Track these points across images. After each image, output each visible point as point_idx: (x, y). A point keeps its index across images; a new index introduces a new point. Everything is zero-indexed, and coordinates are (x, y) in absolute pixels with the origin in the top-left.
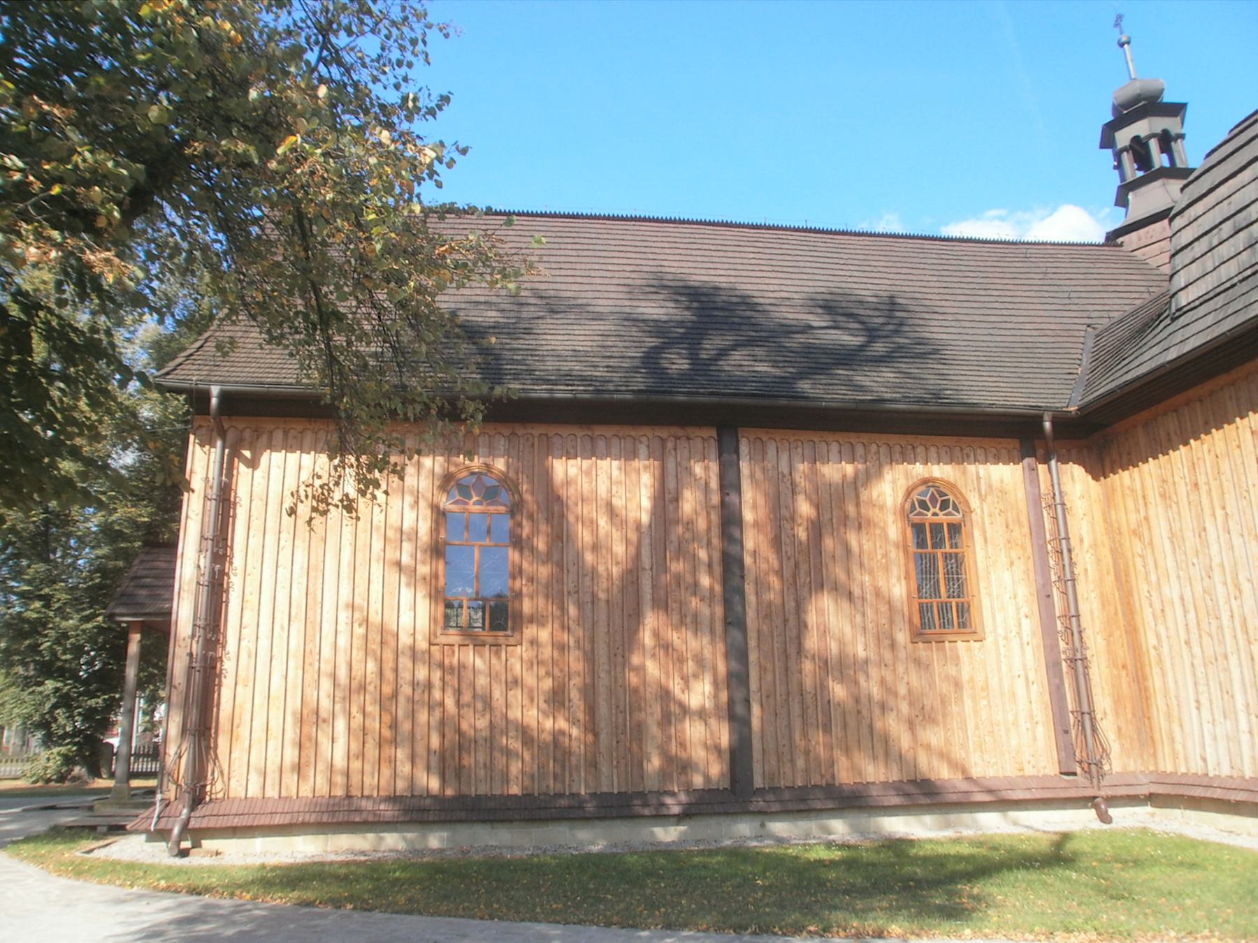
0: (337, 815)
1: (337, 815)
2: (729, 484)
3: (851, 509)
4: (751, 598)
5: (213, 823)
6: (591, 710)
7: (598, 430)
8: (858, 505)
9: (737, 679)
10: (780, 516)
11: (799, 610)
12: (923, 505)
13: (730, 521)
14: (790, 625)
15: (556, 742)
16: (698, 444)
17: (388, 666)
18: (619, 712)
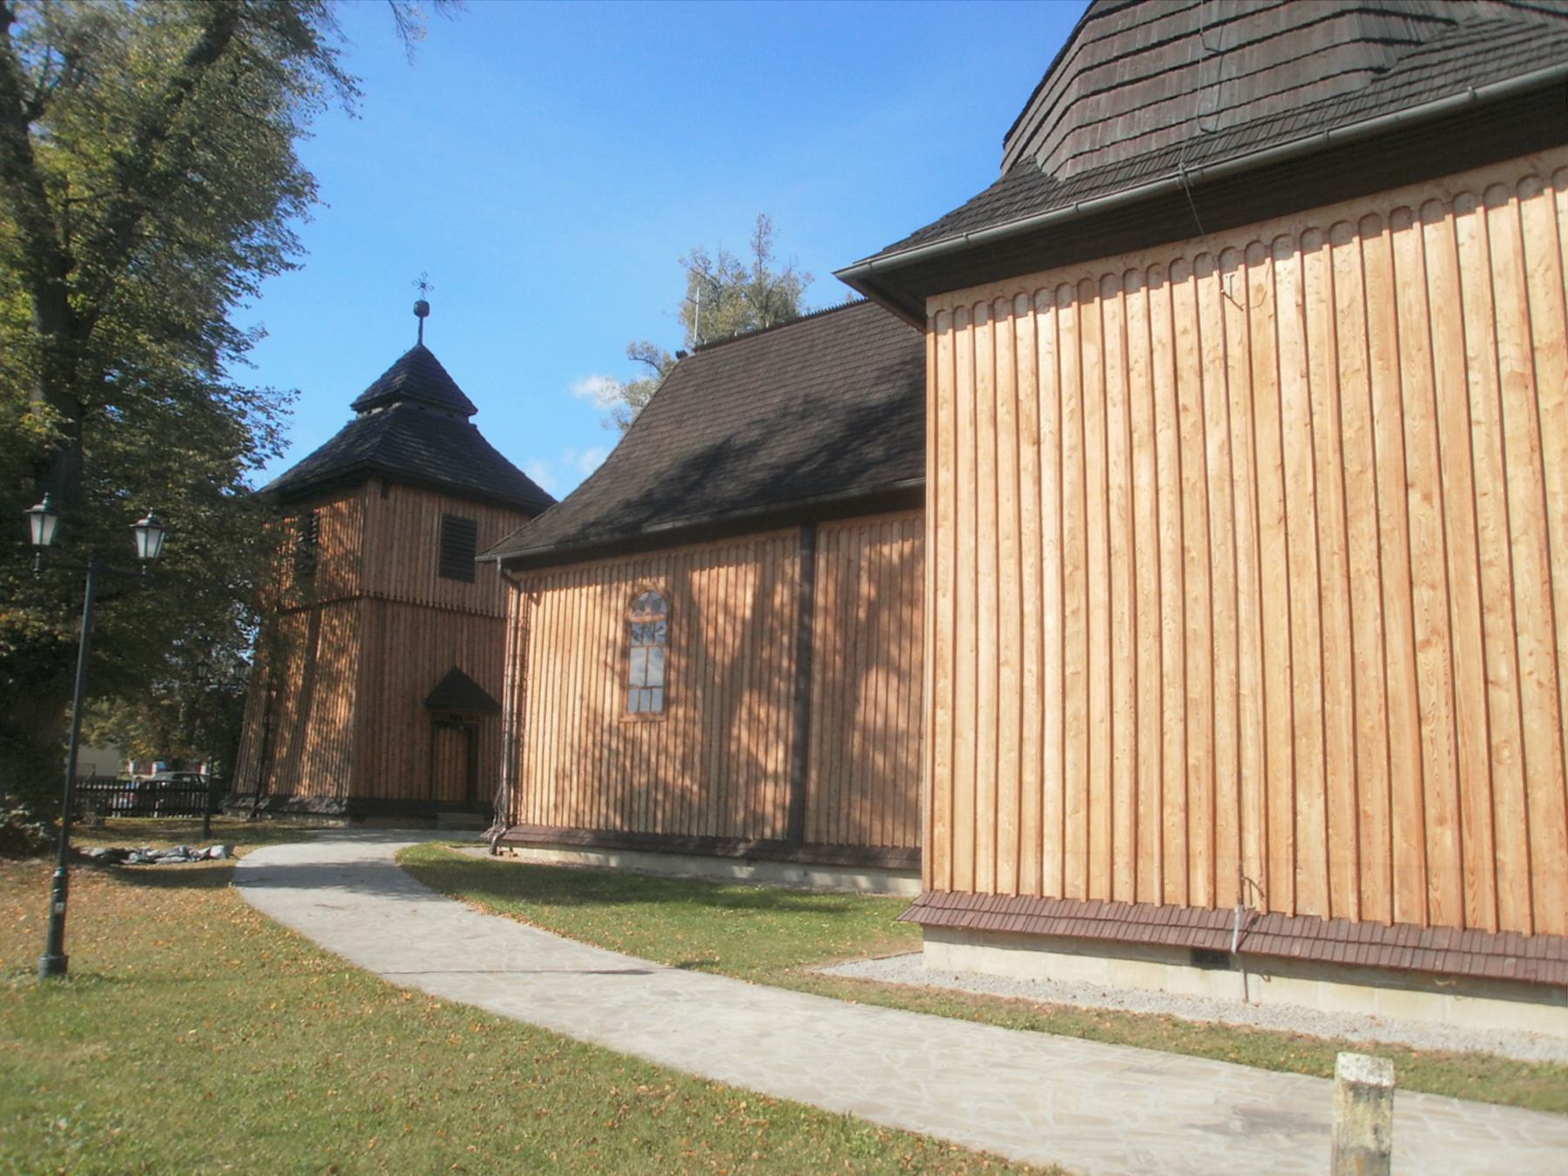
0: (564, 840)
1: (564, 840)
2: (809, 575)
3: (906, 586)
4: (818, 677)
5: (521, 837)
6: (705, 770)
7: (722, 544)
8: (912, 581)
9: (800, 750)
10: (847, 596)
11: (855, 685)
13: (806, 606)
14: (845, 699)
15: (683, 797)
16: (789, 544)
17: (598, 738)
18: (723, 771)
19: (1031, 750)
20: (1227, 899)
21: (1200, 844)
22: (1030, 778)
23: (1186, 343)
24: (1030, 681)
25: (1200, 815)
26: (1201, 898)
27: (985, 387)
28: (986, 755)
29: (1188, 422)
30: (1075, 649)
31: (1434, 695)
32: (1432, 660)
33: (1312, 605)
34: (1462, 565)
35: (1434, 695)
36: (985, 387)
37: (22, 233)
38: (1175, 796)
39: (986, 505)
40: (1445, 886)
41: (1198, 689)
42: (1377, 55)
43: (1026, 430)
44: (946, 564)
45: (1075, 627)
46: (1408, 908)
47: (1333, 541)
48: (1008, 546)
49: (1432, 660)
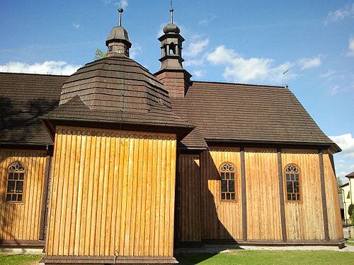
12: (289, 169)
19: (73, 225)
20: (112, 254)
21: (107, 244)
22: (73, 231)
23: (113, 149)
24: (74, 211)
25: (108, 238)
26: (107, 254)
27: (68, 148)
28: (62, 226)
29: (111, 164)
30: (84, 205)
31: (147, 218)
32: (148, 212)
33: (130, 201)
34: (154, 197)
35: (147, 218)
36: (68, 148)
37: (303, 68)
38: (103, 235)
39: (66, 174)
40: (147, 249)
41: (109, 215)
42: (149, 107)
43: (77, 159)
44: (55, 185)
45: (84, 201)
46: (141, 253)
47: (135, 190)
48: (71, 183)
49: (148, 212)
